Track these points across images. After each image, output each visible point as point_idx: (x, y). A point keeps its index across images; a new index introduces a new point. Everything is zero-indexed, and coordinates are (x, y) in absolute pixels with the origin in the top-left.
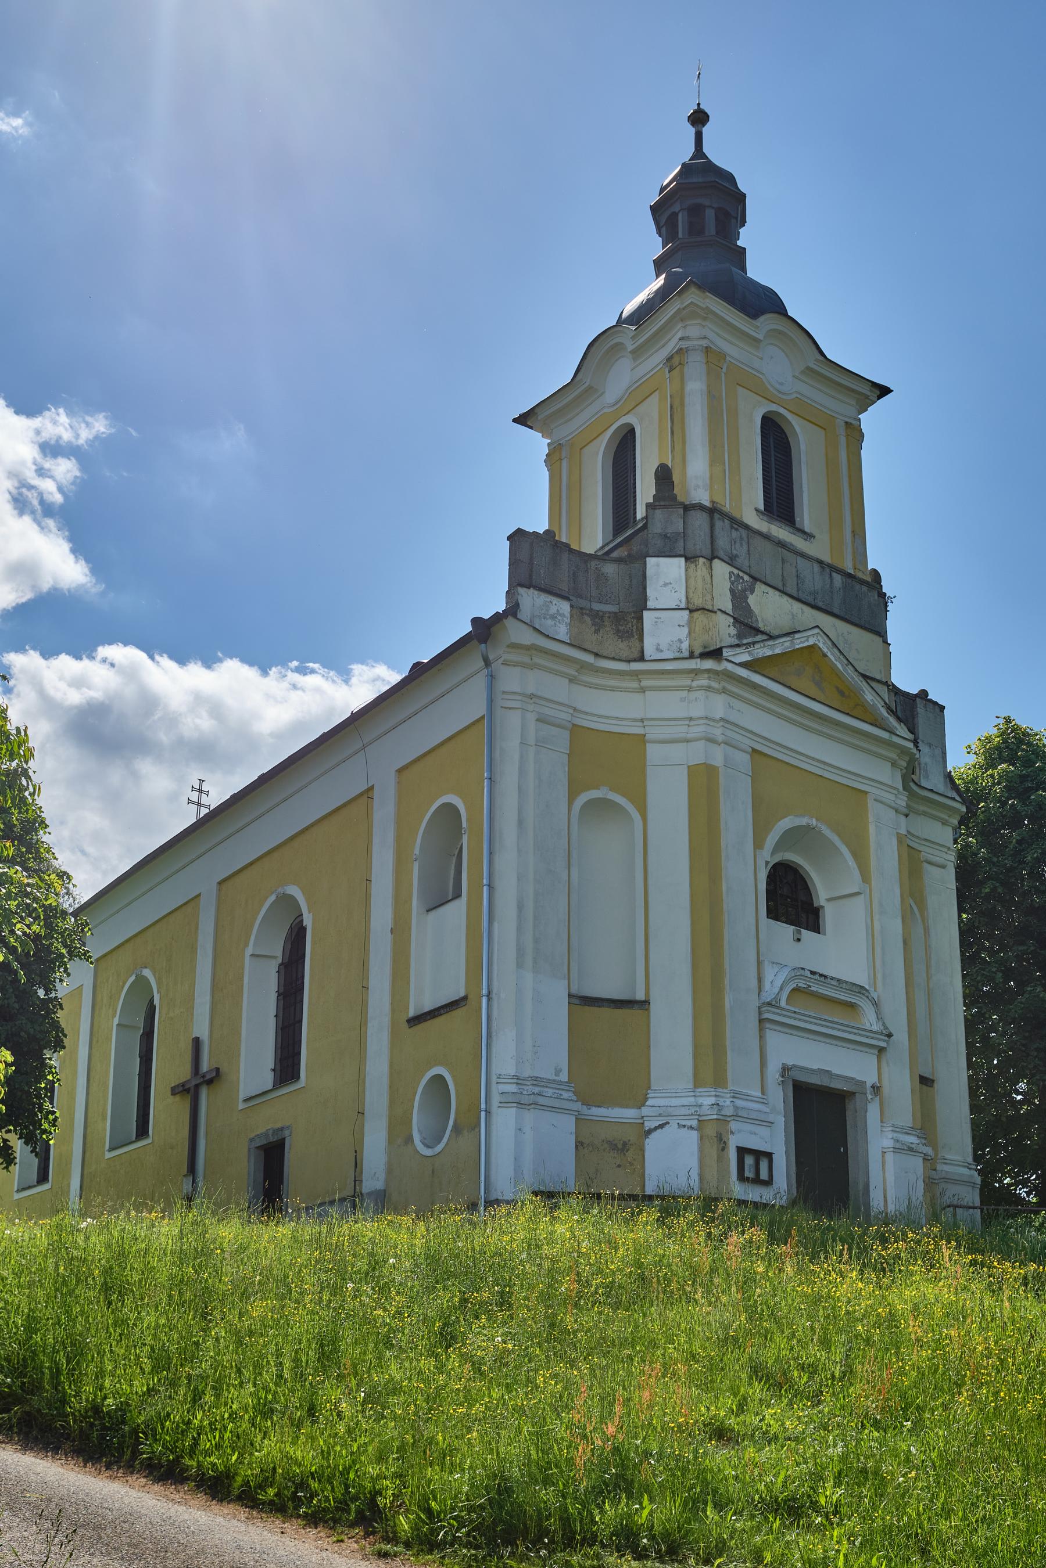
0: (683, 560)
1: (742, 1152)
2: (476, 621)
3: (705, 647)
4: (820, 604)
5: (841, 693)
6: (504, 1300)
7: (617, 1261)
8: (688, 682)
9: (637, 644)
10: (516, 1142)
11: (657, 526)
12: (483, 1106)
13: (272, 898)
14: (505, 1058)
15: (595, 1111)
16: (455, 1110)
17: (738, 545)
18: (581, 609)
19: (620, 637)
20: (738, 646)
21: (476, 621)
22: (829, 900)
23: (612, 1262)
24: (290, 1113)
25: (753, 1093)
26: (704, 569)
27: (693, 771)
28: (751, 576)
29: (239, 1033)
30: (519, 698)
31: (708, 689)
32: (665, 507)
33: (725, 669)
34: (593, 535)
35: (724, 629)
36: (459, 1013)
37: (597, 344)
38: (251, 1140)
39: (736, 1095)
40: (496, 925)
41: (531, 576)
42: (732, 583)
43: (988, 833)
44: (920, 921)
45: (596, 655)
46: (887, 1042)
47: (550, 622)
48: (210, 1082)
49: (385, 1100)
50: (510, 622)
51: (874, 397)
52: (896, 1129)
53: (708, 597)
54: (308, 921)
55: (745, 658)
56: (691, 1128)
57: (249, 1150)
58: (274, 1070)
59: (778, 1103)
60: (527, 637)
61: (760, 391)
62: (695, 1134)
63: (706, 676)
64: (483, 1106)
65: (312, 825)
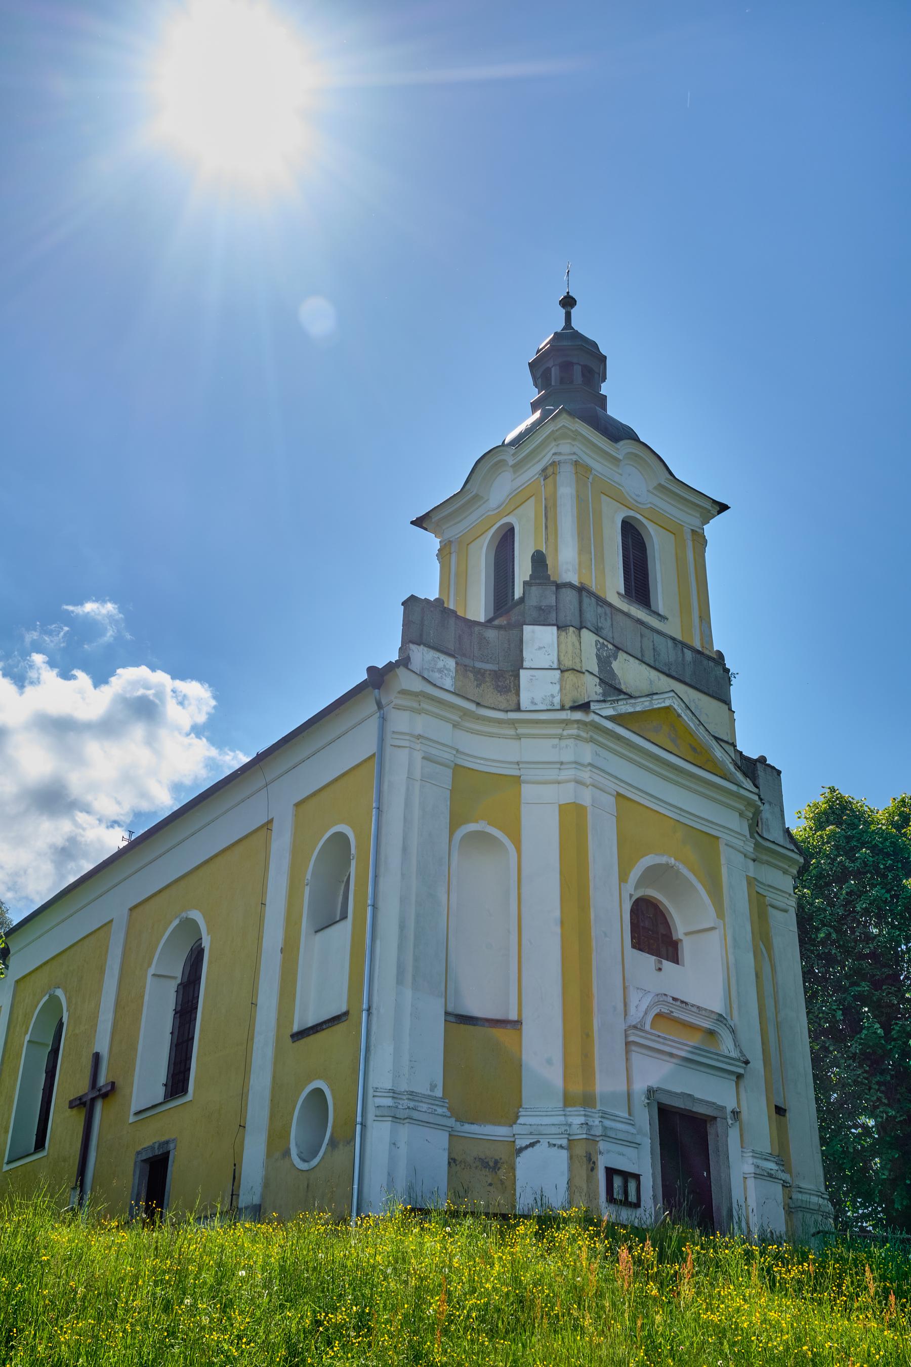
0: (555, 628)
1: (611, 1172)
2: (371, 670)
3: (574, 702)
4: (674, 674)
6: (363, 1323)
7: (494, 1278)
8: (559, 731)
9: (514, 698)
10: (391, 1153)
11: (533, 601)
12: (359, 1119)
13: (176, 922)
14: (382, 1073)
15: (467, 1127)
16: (330, 1123)
17: (602, 619)
19: (499, 691)
20: (604, 701)
21: (371, 670)
22: (686, 934)
23: (488, 1280)
24: (184, 1129)
25: (621, 1114)
26: (574, 637)
27: (563, 809)
28: (614, 645)
29: (136, 1050)
30: (407, 737)
31: (577, 737)
32: (540, 584)
33: (593, 721)
34: (478, 607)
35: (591, 688)
36: (340, 1028)
37: (483, 462)
38: (138, 1153)
39: (604, 1115)
40: (378, 943)
41: (421, 635)
42: (598, 650)
43: (821, 884)
44: (767, 959)
45: (478, 704)
46: (745, 1068)
47: (437, 675)
48: (105, 1096)
49: (266, 1113)
50: (401, 672)
51: (714, 512)
52: (756, 1155)
53: (578, 660)
54: (206, 943)
55: (610, 712)
56: (561, 1147)
57: (136, 1162)
58: (165, 1085)
59: (645, 1122)
60: (417, 685)
62: (564, 1154)
63: (576, 726)
64: (359, 1119)
65: (216, 856)
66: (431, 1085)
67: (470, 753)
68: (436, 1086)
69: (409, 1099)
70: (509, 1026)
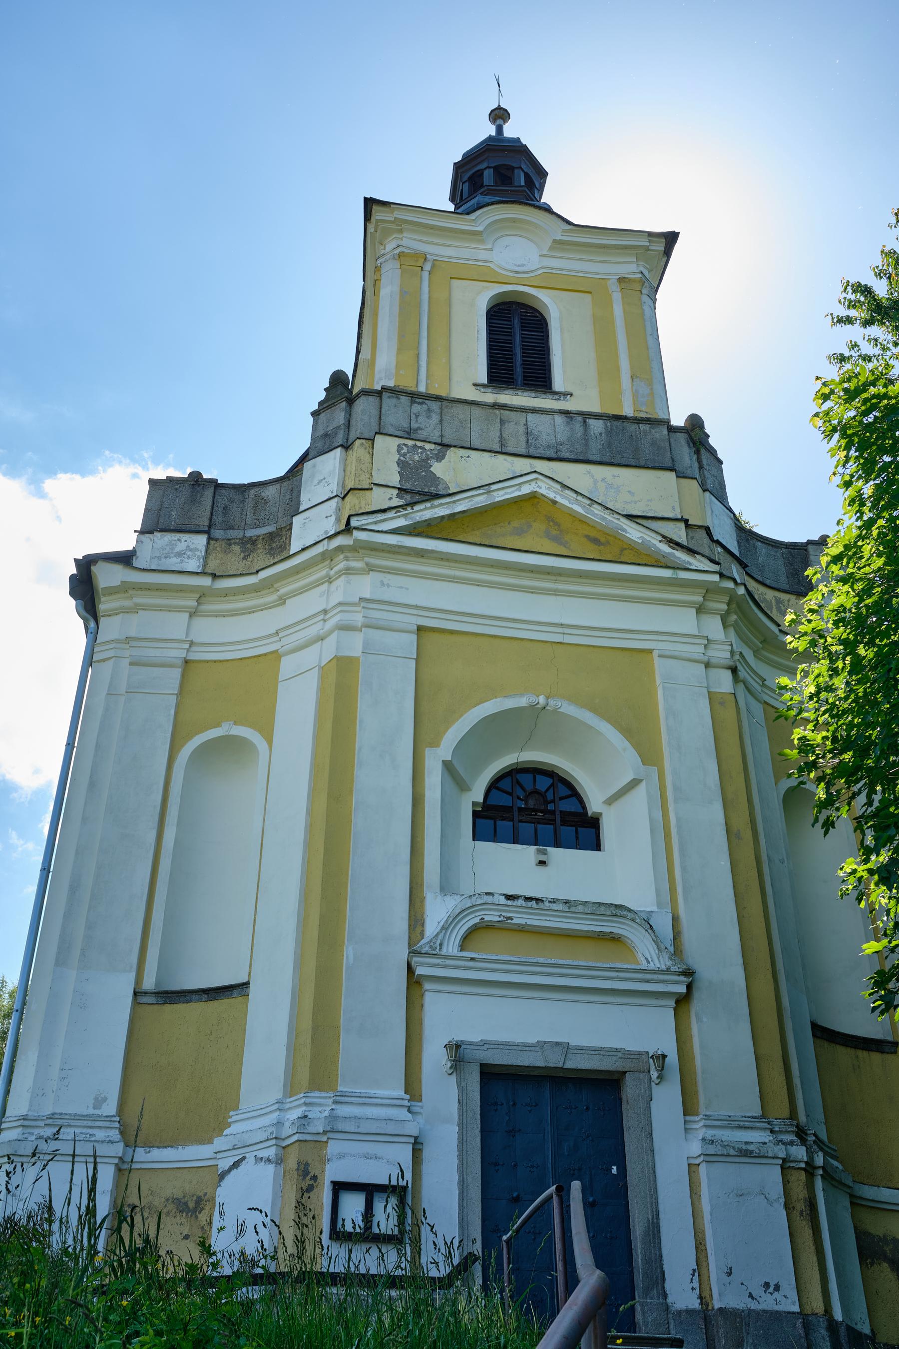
5: (595, 541)
18: (229, 540)
31: (348, 571)
56: (269, 1160)
61: (485, 276)
66: (96, 1099)
67: (221, 641)
68: (105, 1099)
69: (706, 1126)
70: (235, 993)
